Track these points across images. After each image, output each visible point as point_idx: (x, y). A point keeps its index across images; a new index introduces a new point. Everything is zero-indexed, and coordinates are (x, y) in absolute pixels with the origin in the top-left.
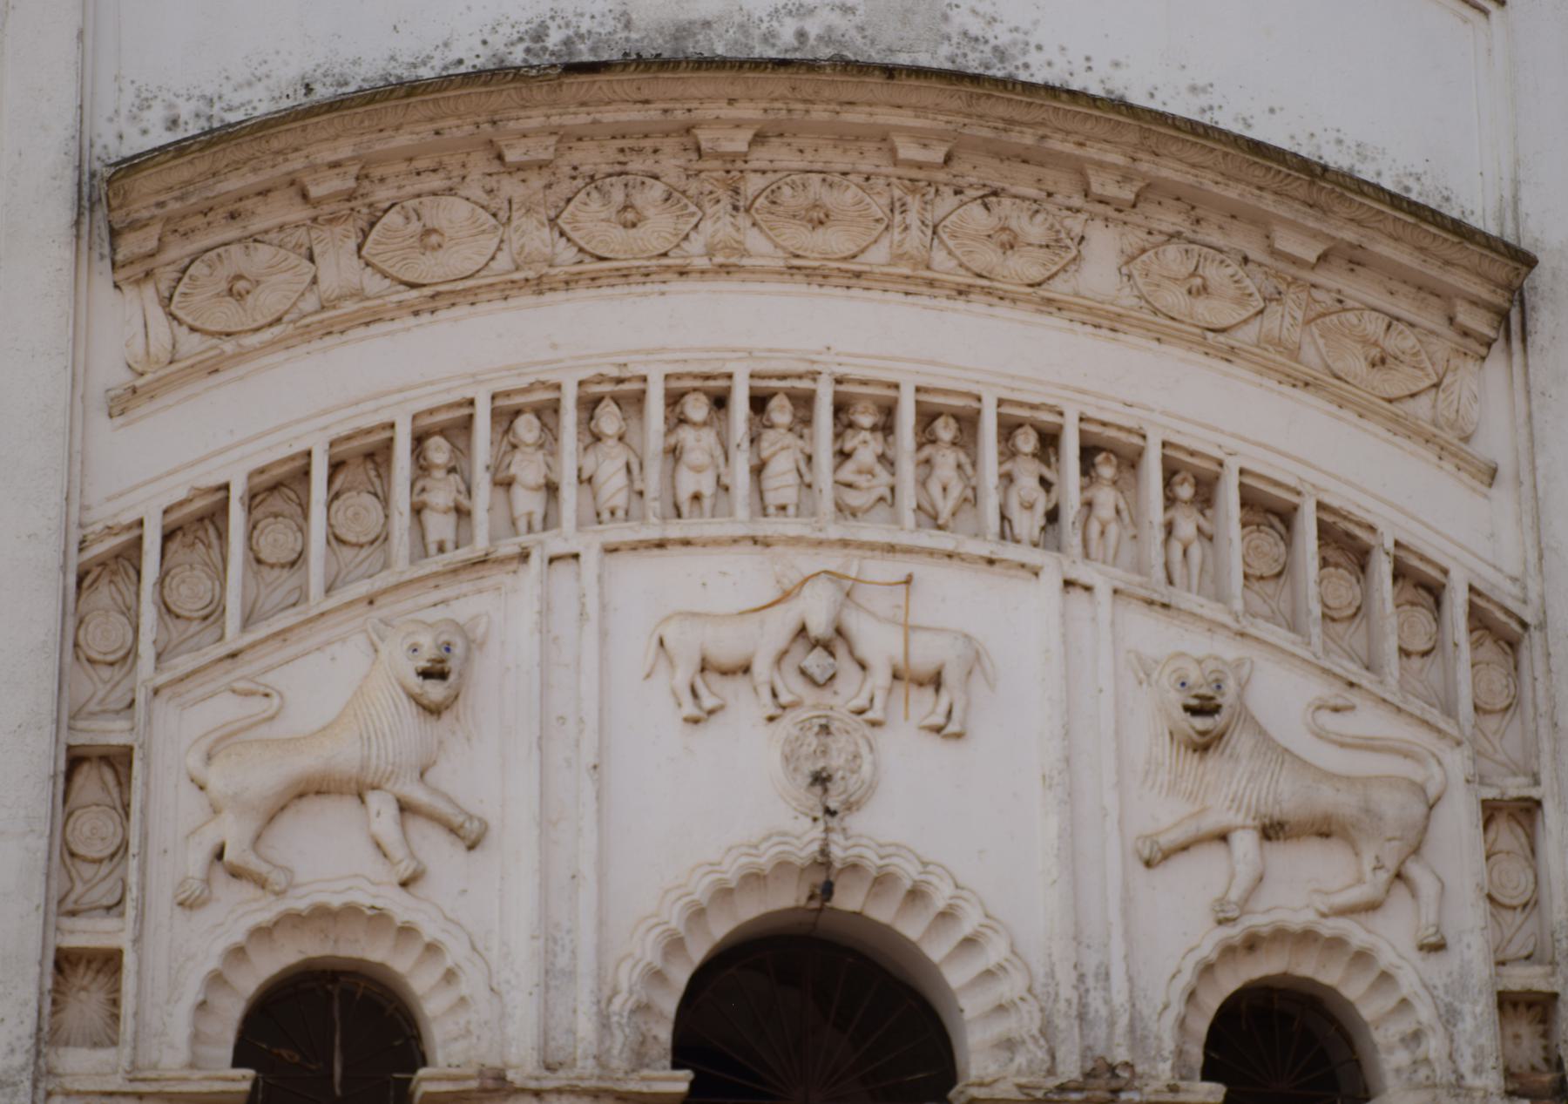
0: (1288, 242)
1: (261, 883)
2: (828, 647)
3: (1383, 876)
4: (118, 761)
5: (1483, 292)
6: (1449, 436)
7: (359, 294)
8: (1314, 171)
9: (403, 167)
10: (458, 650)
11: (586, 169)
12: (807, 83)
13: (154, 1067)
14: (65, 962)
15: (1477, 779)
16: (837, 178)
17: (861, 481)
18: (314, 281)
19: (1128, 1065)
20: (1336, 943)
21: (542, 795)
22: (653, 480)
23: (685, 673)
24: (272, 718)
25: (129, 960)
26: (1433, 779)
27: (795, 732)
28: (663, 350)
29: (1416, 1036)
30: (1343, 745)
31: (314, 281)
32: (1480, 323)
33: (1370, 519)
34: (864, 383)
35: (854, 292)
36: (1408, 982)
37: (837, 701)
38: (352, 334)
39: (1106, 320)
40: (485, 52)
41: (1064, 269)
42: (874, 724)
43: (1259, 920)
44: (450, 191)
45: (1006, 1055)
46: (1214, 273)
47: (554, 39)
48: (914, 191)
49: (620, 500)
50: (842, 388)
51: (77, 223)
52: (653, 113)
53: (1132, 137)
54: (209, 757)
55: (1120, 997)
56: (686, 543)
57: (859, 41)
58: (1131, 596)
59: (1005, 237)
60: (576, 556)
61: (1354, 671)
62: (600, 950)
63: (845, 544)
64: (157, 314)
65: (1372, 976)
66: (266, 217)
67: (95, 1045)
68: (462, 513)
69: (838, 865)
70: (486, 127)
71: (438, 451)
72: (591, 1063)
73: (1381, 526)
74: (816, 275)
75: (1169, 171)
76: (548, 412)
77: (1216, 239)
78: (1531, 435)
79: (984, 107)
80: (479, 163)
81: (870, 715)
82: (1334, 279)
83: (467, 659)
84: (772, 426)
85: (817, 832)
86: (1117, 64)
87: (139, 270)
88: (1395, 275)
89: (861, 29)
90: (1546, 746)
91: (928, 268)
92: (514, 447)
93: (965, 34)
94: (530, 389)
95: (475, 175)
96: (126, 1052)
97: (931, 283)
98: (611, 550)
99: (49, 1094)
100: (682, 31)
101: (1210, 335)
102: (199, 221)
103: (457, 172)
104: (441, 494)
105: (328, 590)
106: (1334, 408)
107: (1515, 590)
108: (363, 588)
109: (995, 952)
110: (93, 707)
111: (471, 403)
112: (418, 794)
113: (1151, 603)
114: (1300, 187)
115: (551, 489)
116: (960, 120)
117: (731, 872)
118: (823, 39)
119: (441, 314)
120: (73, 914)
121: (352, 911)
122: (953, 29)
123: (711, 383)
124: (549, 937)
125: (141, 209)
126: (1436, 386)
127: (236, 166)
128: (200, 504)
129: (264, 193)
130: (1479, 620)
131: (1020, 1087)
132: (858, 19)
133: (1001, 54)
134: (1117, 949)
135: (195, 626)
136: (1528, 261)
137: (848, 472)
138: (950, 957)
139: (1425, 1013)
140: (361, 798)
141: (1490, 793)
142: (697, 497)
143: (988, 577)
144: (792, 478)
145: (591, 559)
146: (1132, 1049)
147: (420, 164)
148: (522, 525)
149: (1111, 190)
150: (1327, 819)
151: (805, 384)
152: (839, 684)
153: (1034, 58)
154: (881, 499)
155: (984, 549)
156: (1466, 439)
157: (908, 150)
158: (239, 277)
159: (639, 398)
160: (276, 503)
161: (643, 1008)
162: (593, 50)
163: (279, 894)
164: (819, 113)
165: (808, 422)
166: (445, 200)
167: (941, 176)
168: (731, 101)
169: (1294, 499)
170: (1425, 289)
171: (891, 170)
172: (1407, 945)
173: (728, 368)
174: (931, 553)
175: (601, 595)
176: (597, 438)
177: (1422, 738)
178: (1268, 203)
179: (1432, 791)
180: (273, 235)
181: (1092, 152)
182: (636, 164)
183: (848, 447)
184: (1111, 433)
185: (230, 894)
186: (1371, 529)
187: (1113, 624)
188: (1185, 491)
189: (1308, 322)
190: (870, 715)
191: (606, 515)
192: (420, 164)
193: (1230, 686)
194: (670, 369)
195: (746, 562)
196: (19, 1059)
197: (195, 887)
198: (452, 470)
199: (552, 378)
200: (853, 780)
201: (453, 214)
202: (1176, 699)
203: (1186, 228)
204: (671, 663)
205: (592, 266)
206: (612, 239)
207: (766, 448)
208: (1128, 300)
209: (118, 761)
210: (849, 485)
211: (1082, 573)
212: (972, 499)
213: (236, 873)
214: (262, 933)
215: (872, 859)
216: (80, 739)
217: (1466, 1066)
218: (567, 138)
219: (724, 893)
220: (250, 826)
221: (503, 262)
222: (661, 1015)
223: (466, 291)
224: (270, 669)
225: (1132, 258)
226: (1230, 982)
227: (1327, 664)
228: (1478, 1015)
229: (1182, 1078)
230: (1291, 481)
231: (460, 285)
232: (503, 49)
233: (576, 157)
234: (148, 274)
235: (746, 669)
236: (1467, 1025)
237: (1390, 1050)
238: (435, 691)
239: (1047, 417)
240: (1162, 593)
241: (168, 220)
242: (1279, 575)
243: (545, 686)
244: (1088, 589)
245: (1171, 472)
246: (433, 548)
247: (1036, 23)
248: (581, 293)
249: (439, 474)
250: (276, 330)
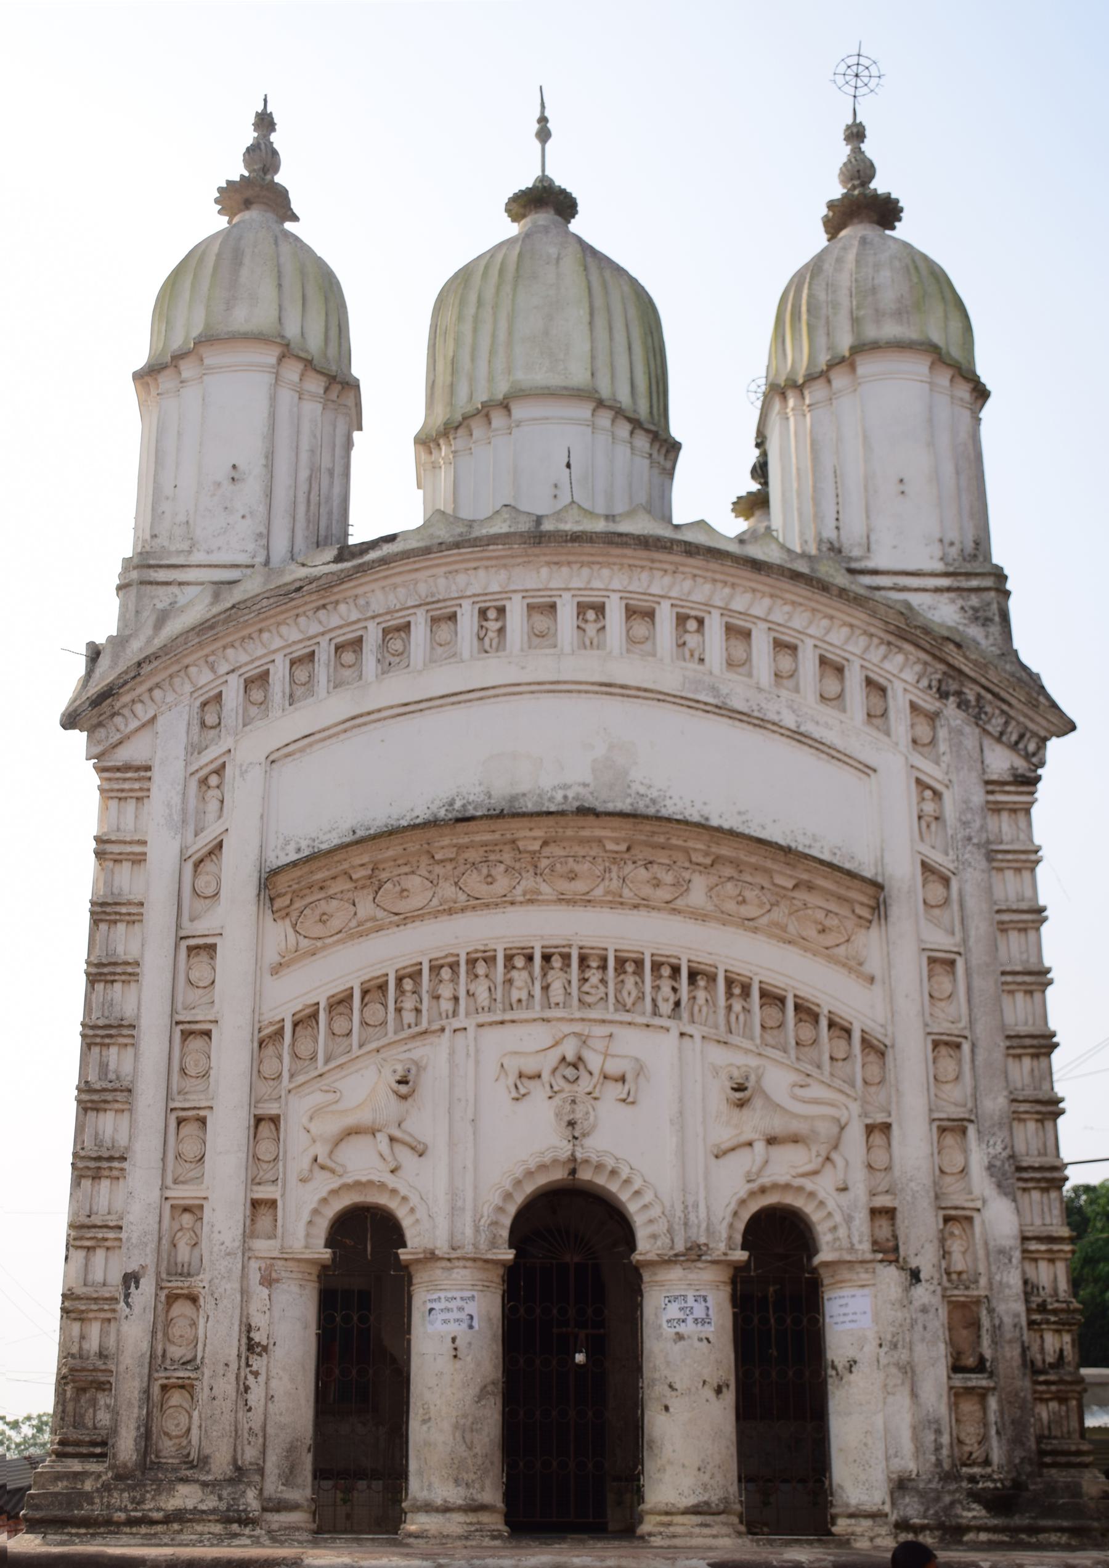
29: (834, 1228)
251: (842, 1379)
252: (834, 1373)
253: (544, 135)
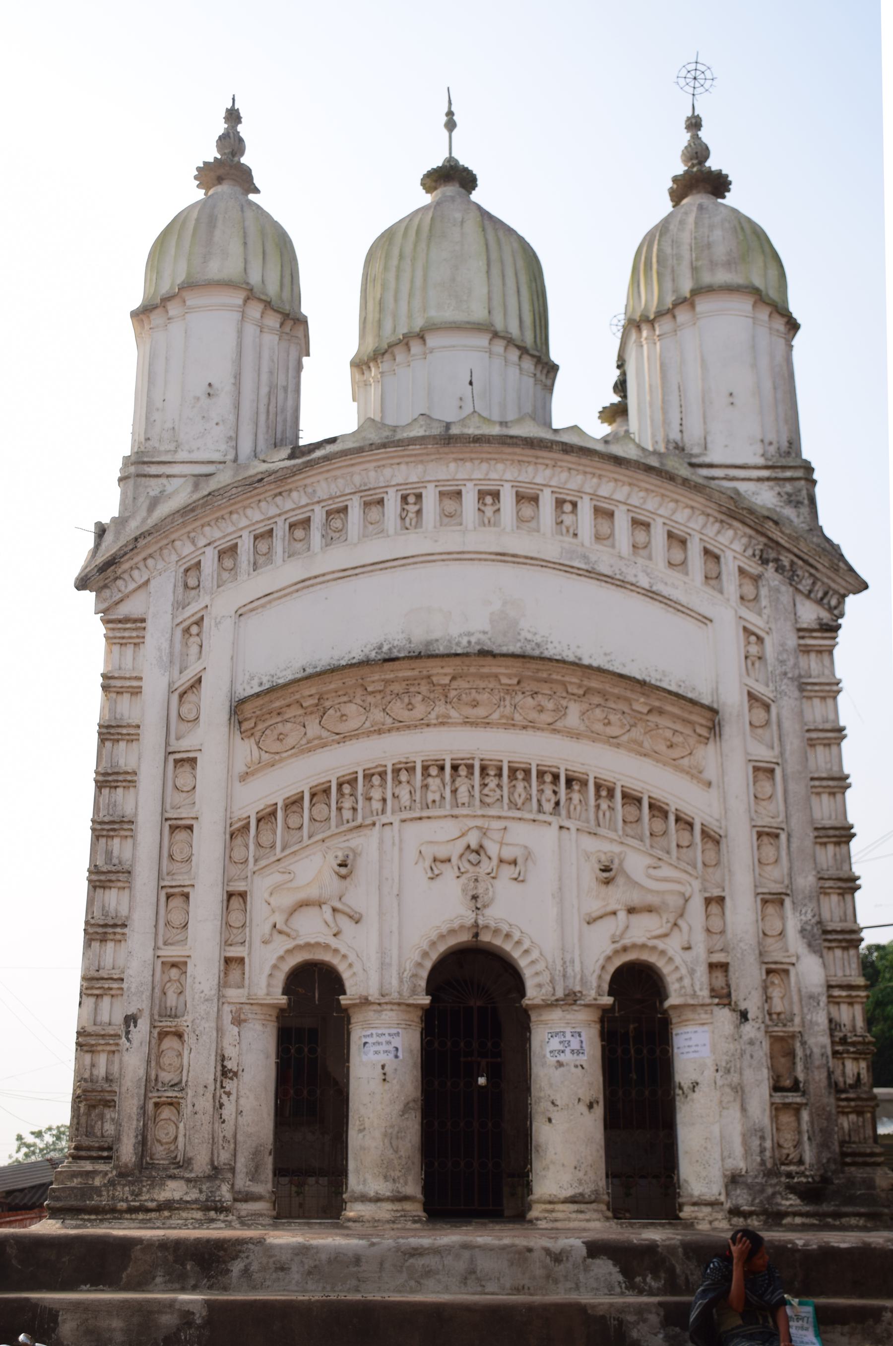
0: (637, 707)
1: (288, 935)
2: (478, 853)
3: (669, 925)
4: (243, 895)
5: (704, 722)
6: (694, 772)
7: (320, 738)
8: (643, 683)
9: (334, 694)
10: (351, 857)
11: (396, 692)
12: (467, 661)
13: (256, 995)
14: (228, 961)
15: (705, 890)
16: (481, 691)
17: (491, 794)
18: (305, 734)
19: (580, 992)
20: (654, 948)
21: (380, 905)
22: (418, 797)
23: (428, 862)
24: (291, 881)
25: (247, 960)
26: (688, 891)
27: (466, 881)
28: (422, 752)
29: (681, 979)
30: (657, 880)
31: (305, 734)
32: (704, 732)
33: (666, 801)
34: (491, 760)
35: (488, 729)
36: (678, 961)
37: (481, 870)
38: (318, 751)
39: (574, 735)
40: (362, 654)
41: (560, 718)
42: (493, 878)
43: (627, 941)
44: (350, 701)
45: (538, 989)
46: (613, 718)
47: (385, 648)
48: (507, 694)
49: (408, 804)
50: (483, 762)
51: (230, 719)
52: (416, 673)
53: (580, 673)
54: (271, 894)
55: (577, 968)
56: (429, 818)
57: (489, 643)
58: (583, 831)
59: (539, 708)
60: (391, 824)
61: (660, 854)
62: (400, 957)
63: (483, 816)
64: (255, 747)
65: (666, 959)
66: (289, 713)
67: (239, 987)
68: (354, 809)
69: (481, 926)
70: (360, 681)
71: (347, 789)
72: (396, 994)
73: (671, 803)
74: (474, 724)
75: (594, 684)
76: (382, 775)
77: (613, 706)
78: (723, 770)
79: (528, 665)
80: (359, 692)
81: (492, 875)
82: (654, 718)
83: (354, 859)
84: (460, 776)
85: (474, 915)
86: (578, 647)
87: (249, 733)
88: (675, 717)
89: (490, 639)
90: (727, 878)
91: (513, 720)
92: (372, 786)
93: (526, 639)
94: (376, 767)
95: (358, 695)
96: (246, 990)
97: (514, 725)
98: (403, 821)
99: (223, 1003)
100: (429, 643)
101: (611, 740)
102: (268, 716)
103: (352, 695)
104: (347, 804)
105: (310, 837)
106: (655, 763)
107: (717, 824)
108: (319, 837)
109: (535, 955)
110: (236, 877)
111: (356, 772)
112: (338, 905)
113: (590, 833)
114: (638, 688)
115: (384, 800)
116: (521, 670)
117: (444, 929)
118: (478, 643)
119: (347, 743)
120: (231, 945)
121: (318, 944)
122: (521, 637)
123: (438, 763)
124: (383, 953)
125: (248, 715)
126: (690, 754)
127: (278, 699)
128: (268, 810)
129: (289, 706)
130: (705, 834)
131: (543, 1000)
132: (489, 636)
133: (538, 645)
134: (577, 953)
135: (268, 850)
136: (715, 712)
137: (486, 791)
138: (521, 956)
139: (683, 971)
140: (320, 906)
141: (707, 895)
142: (434, 801)
143: (531, 827)
144: (467, 794)
145: (396, 824)
146: (582, 986)
147: (340, 693)
148: (375, 813)
149: (575, 691)
150: (650, 906)
151: (470, 762)
152: (481, 865)
153: (550, 646)
154: (498, 800)
155: (532, 816)
156: (700, 772)
157: (505, 680)
158: (281, 734)
159: (414, 768)
160: (294, 808)
161: (415, 976)
162: (399, 651)
163: (294, 939)
164: (473, 670)
165: (472, 774)
166: (349, 705)
167: (517, 688)
168: (442, 667)
169: (640, 795)
170: (685, 721)
171: (499, 687)
172: (678, 947)
173: (443, 757)
174: (514, 818)
175: (400, 836)
176: (400, 782)
177: (684, 876)
178: (629, 694)
179: (687, 895)
180: (292, 720)
181: (567, 679)
182: (412, 689)
183: (486, 782)
184: (577, 774)
185: (278, 939)
186: (667, 804)
187: (577, 841)
188: (604, 793)
189: (646, 733)
190: (492, 875)
191: (403, 809)
192: (340, 693)
193: (616, 862)
194: (423, 758)
195: (449, 824)
196: (213, 992)
197: (267, 937)
198: (351, 795)
199: (383, 763)
200: (486, 897)
201: (351, 709)
202: (597, 867)
203: (602, 702)
204: (424, 859)
205: (397, 725)
206: (405, 715)
207: (457, 784)
208: (582, 728)
209: (243, 895)
210: (487, 795)
211: (566, 823)
212: (529, 799)
213: (280, 932)
214: (289, 951)
215: (492, 924)
216: (230, 889)
217: (697, 988)
218: (387, 682)
219: (442, 937)
220: (284, 917)
221: (368, 724)
222: (421, 978)
223: (354, 735)
224: (291, 864)
225: (584, 714)
226: (618, 962)
227: (651, 852)
228: (702, 971)
229: (599, 995)
230: (639, 789)
231: (353, 733)
232: (368, 653)
233: (392, 688)
234: (252, 734)
235: (449, 860)
236: (698, 974)
237: (673, 983)
238: (343, 871)
239: (554, 770)
240: (594, 829)
241: (257, 717)
242: (637, 821)
243: (381, 868)
244: (568, 829)
245: (598, 787)
246: (345, 822)
247: (550, 634)
248: (394, 734)
249: (347, 797)
250: (293, 751)
251: (687, 1097)
252: (680, 1092)
253: (451, 125)
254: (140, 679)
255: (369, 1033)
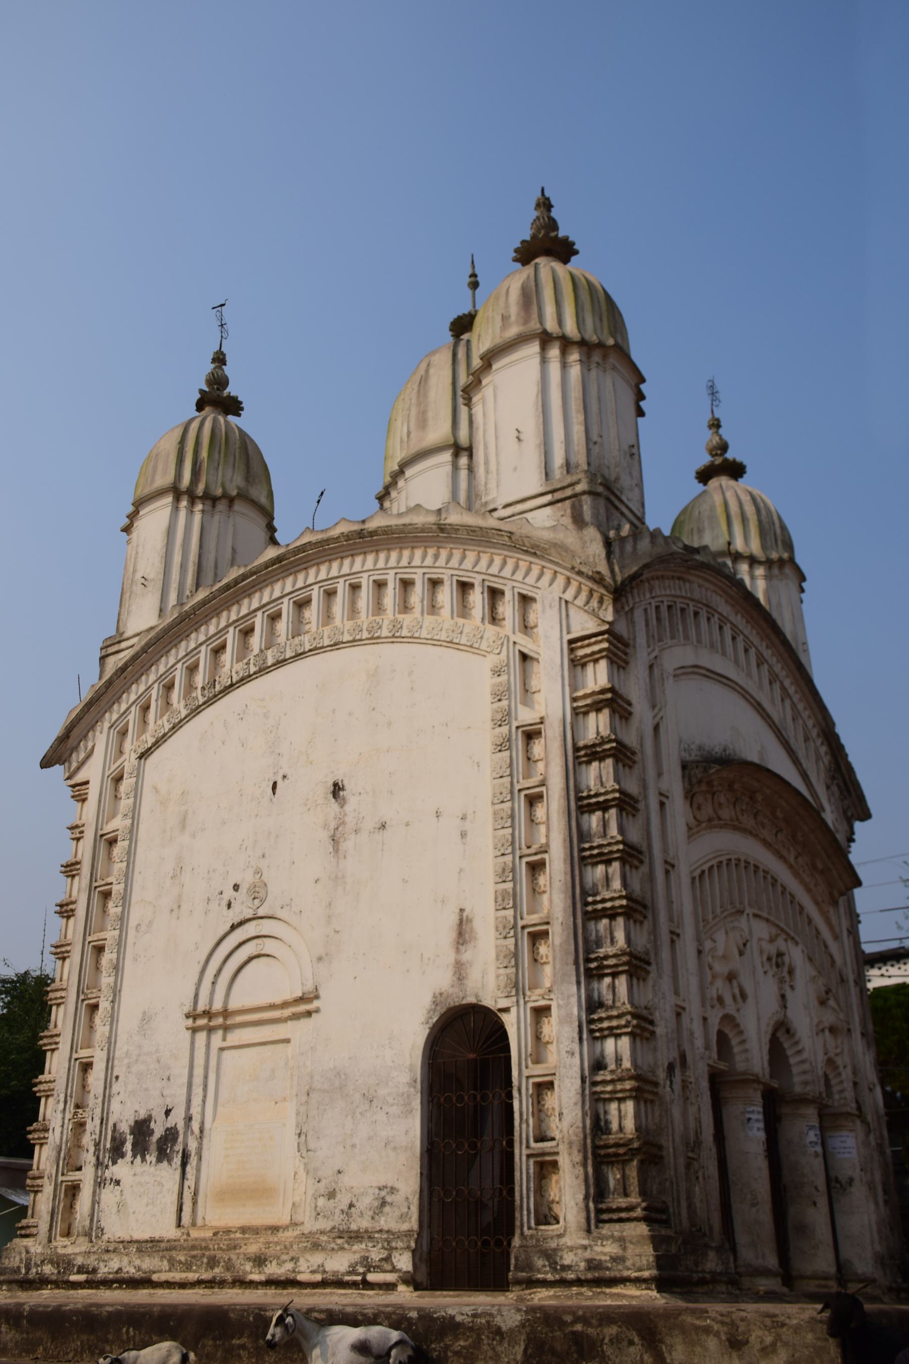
29: (841, 1092)
251: (845, 1190)
253: (474, 285)
254: (73, 797)
255: (751, 1109)
